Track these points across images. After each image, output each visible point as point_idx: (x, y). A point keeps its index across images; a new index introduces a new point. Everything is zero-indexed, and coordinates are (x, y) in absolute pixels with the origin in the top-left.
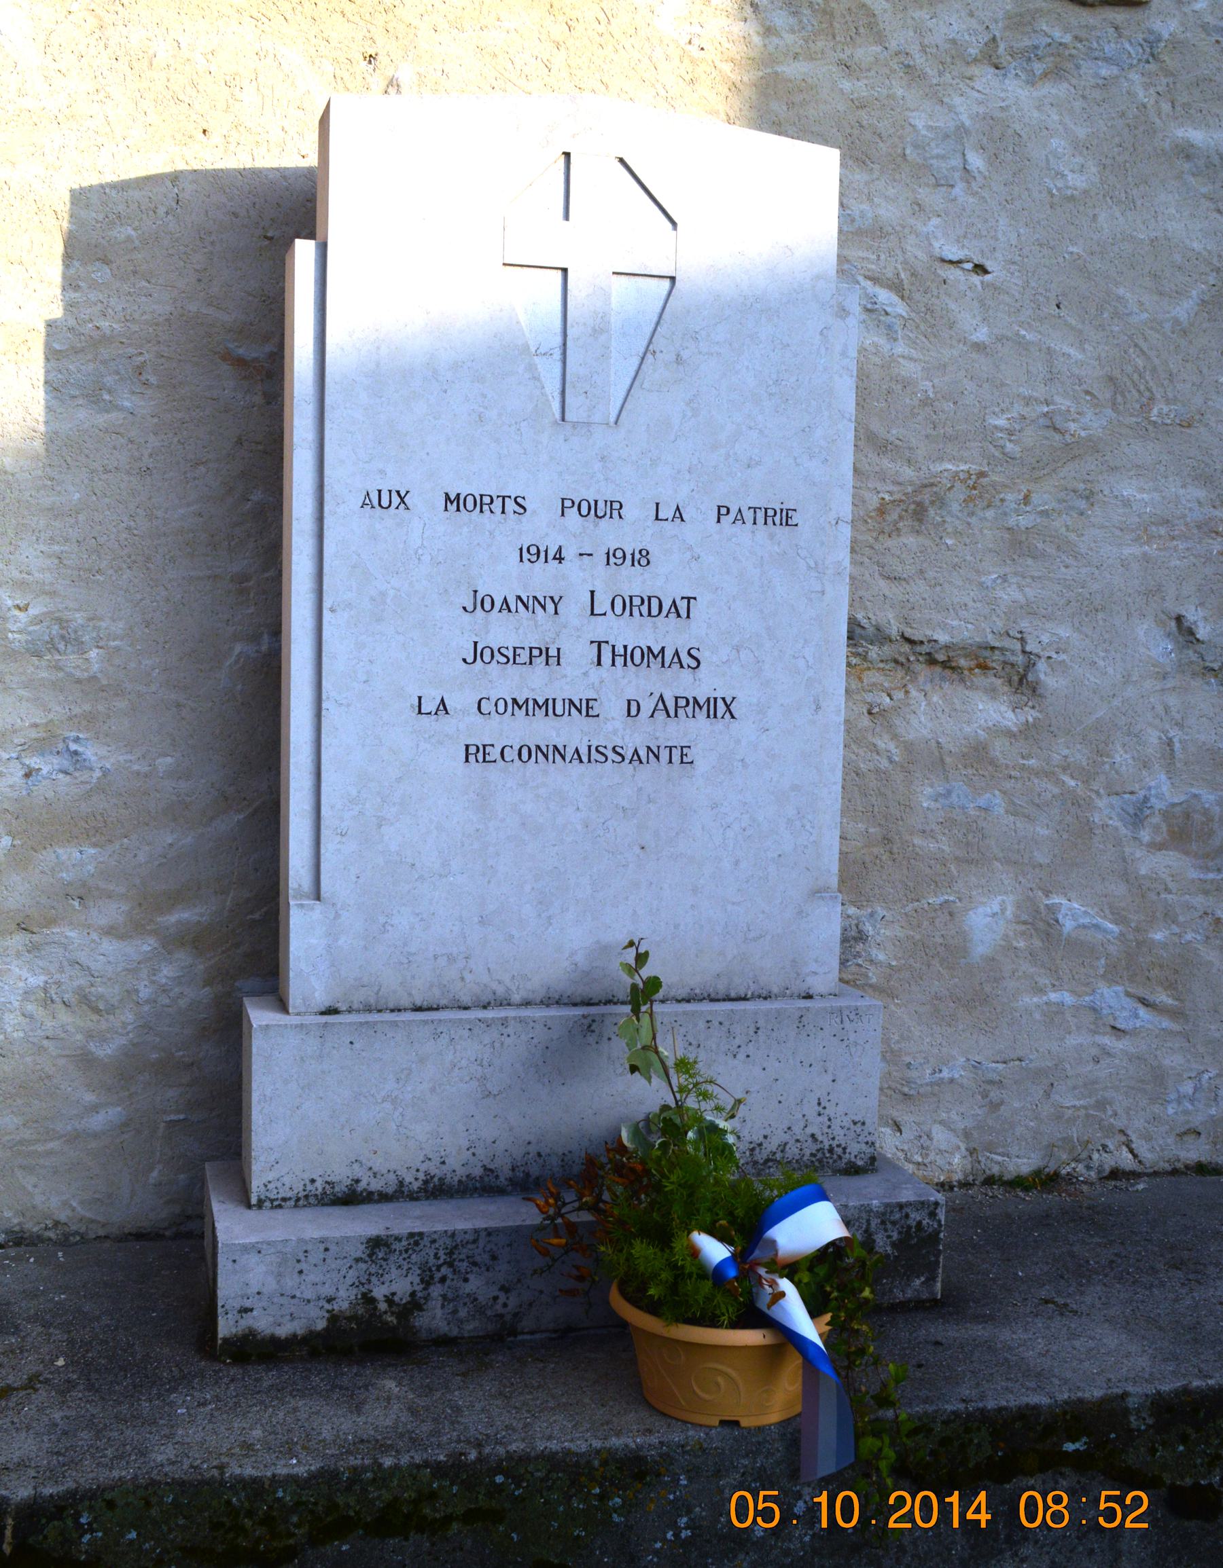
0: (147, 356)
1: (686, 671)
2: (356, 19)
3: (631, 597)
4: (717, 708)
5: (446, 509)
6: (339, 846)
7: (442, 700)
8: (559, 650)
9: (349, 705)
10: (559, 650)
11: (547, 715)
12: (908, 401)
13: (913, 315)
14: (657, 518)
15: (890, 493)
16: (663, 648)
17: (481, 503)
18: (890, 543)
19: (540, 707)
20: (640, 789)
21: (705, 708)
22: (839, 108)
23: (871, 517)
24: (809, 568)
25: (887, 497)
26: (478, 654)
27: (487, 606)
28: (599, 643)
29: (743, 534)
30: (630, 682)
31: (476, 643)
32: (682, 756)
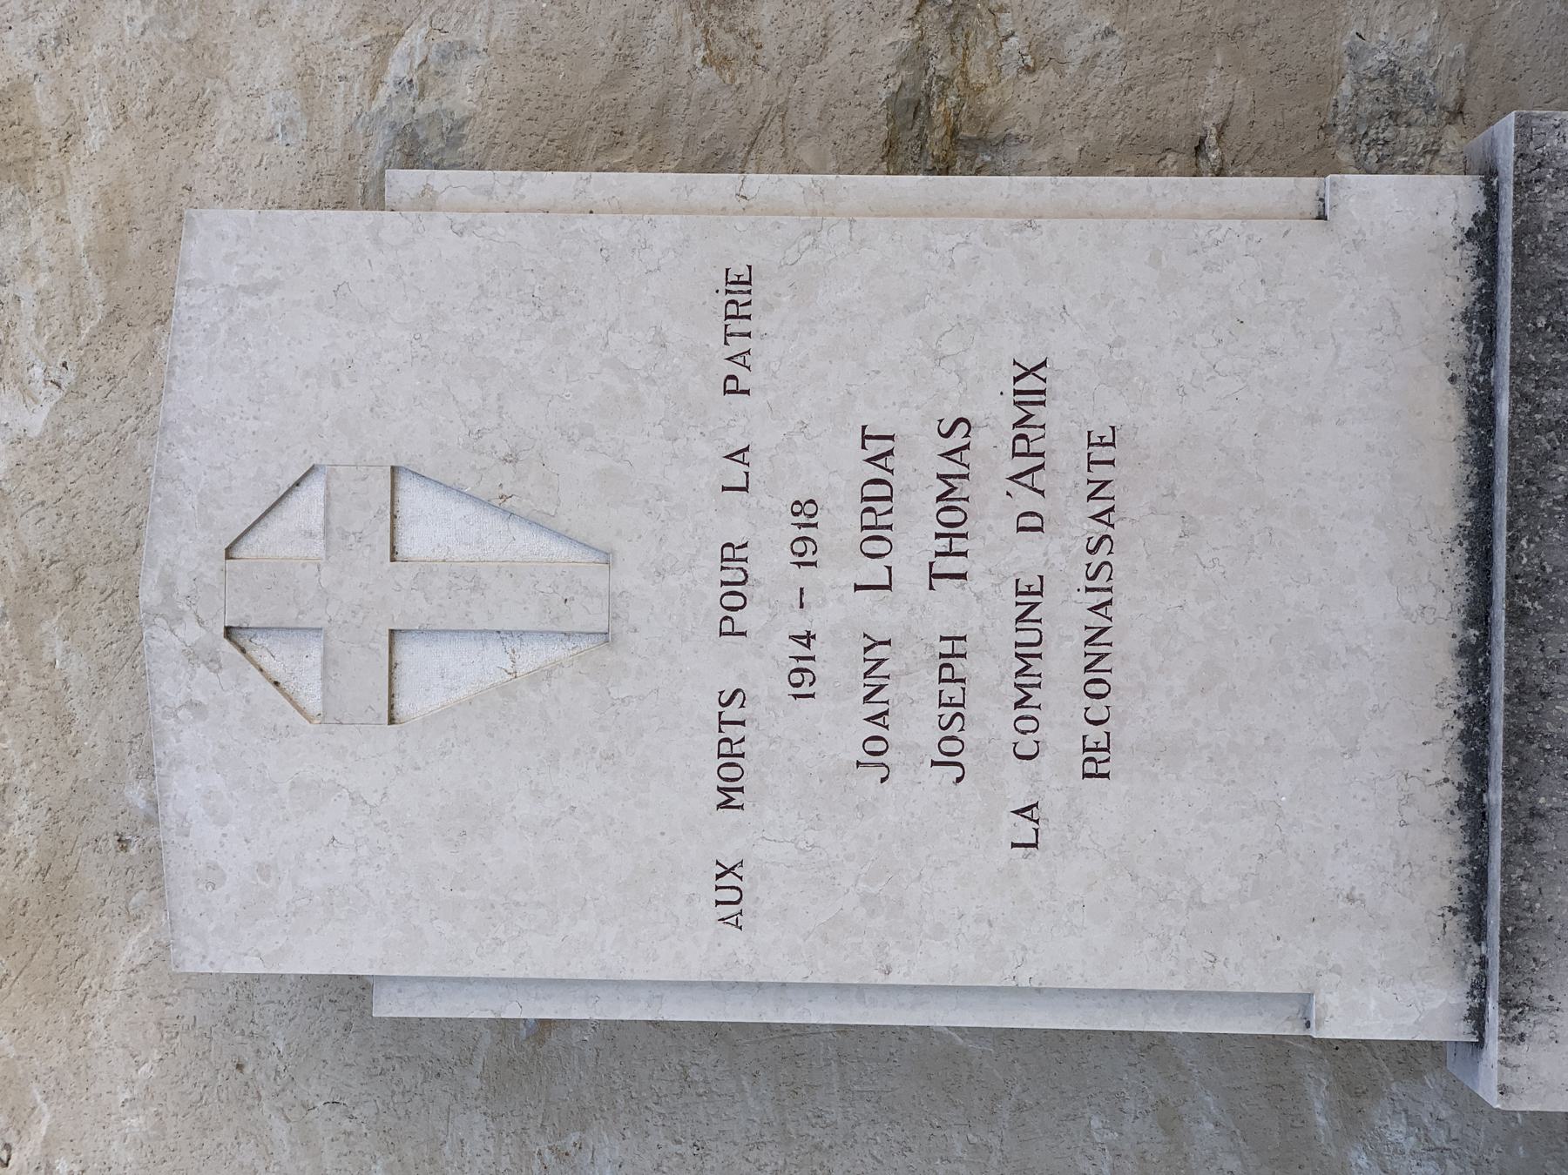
0: (544, 1146)
1: (974, 439)
2: (72, 860)
3: (864, 528)
4: (1030, 389)
5: (741, 807)
6: (1231, 967)
7: (1016, 812)
8: (942, 639)
9: (1024, 948)
10: (942, 639)
11: (1039, 656)
12: (554, 23)
13: (424, 17)
14: (745, 489)
15: (695, 47)
16: (939, 476)
17: (730, 756)
18: (770, 48)
19: (1028, 666)
20: (1153, 511)
21: (1029, 408)
22: (129, 149)
23: (733, 79)
24: (814, 245)
25: (701, 54)
26: (949, 760)
27: (880, 746)
28: (933, 576)
29: (765, 353)
30: (990, 528)
31: (934, 763)
32: (1102, 445)
